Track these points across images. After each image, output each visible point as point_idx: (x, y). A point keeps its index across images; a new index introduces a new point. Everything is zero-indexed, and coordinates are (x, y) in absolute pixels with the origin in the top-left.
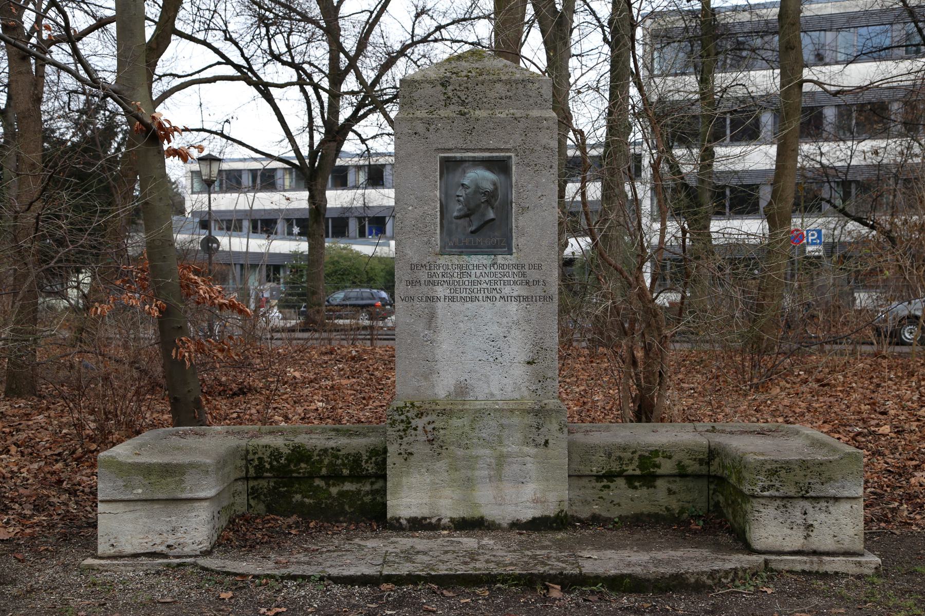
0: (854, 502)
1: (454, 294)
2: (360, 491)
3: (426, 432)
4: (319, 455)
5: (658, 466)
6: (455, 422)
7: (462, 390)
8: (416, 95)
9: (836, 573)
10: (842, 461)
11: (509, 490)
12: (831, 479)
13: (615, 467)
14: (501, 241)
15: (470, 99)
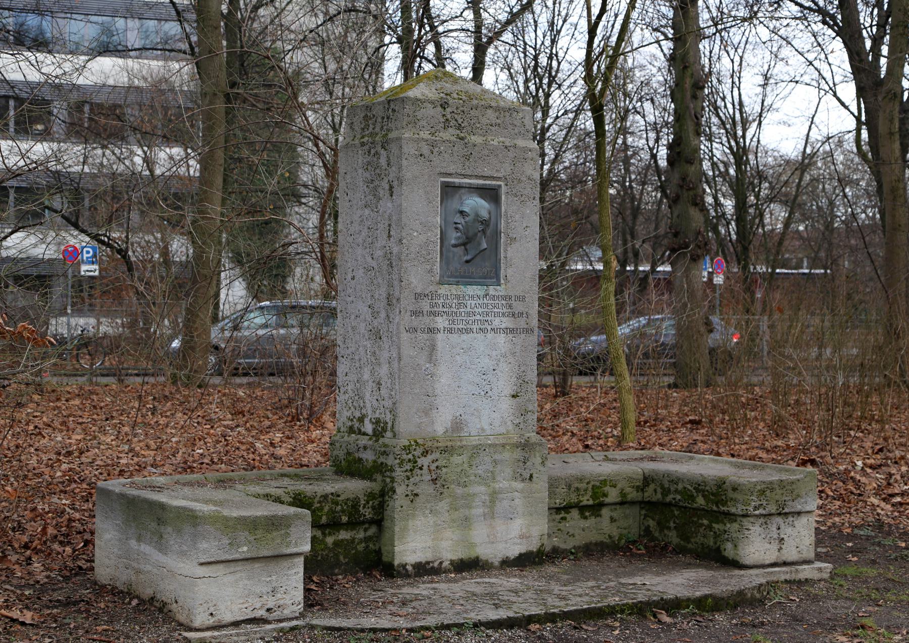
0: (810, 515)
1: (453, 326)
2: (354, 539)
3: (430, 470)
4: (319, 502)
5: (605, 495)
6: (456, 459)
7: (458, 425)
8: (419, 114)
9: (806, 579)
10: (806, 480)
11: (500, 526)
12: (798, 496)
13: (574, 499)
14: (491, 271)
15: (465, 124)
